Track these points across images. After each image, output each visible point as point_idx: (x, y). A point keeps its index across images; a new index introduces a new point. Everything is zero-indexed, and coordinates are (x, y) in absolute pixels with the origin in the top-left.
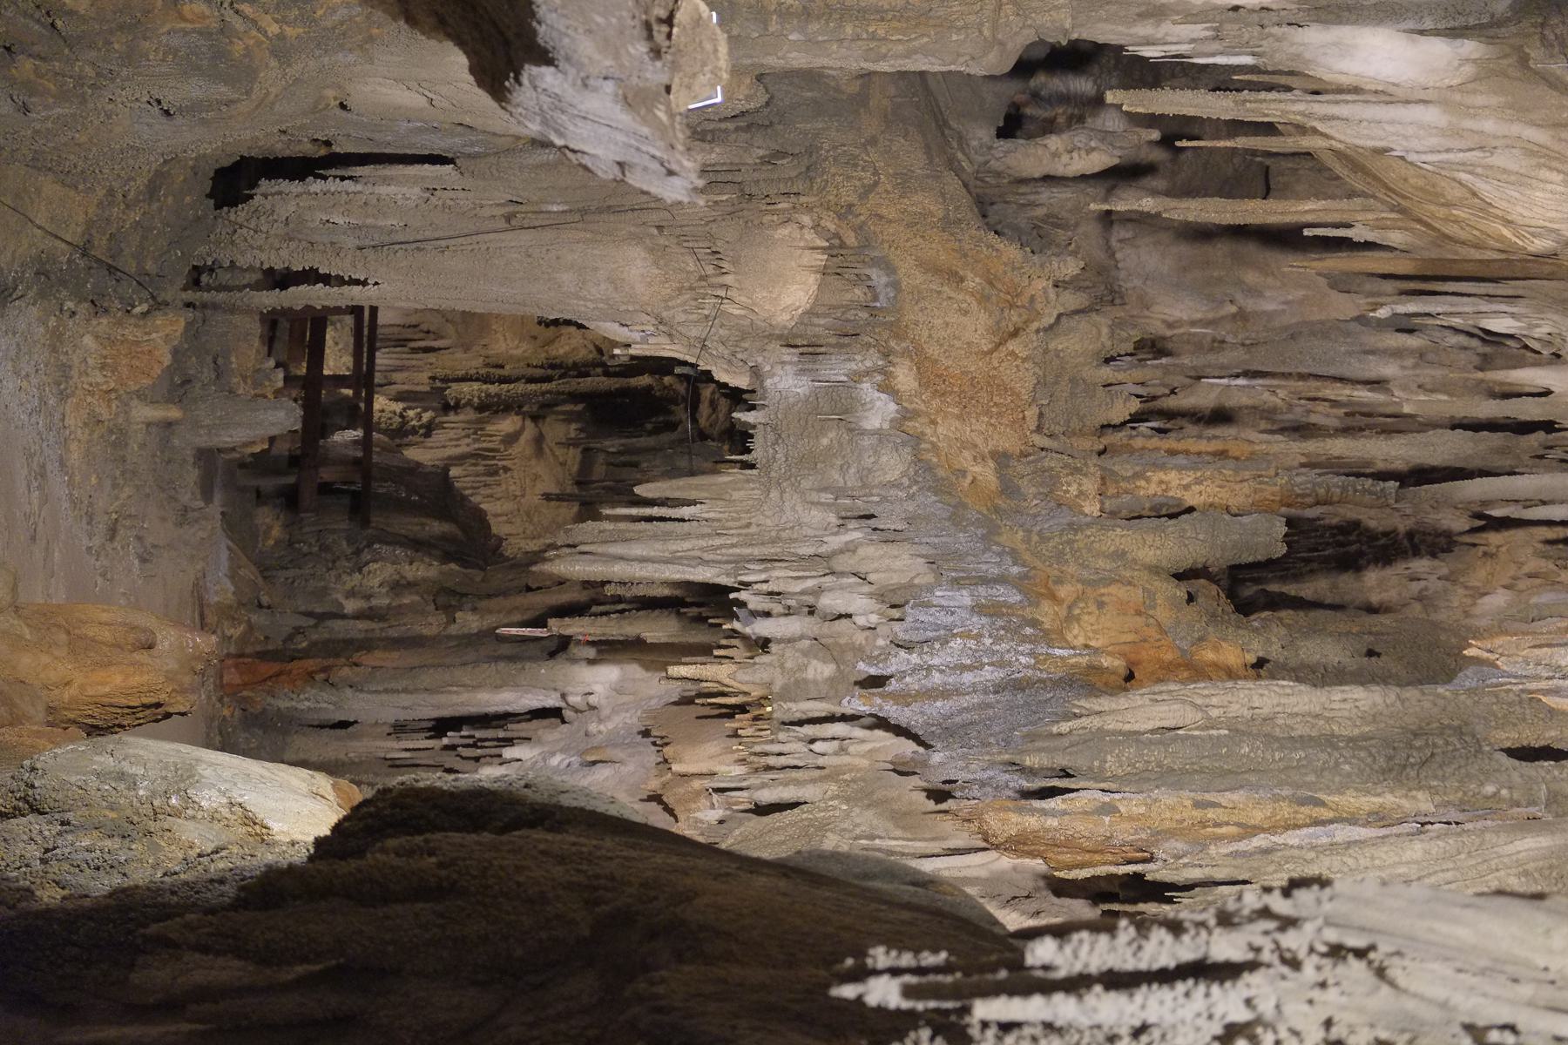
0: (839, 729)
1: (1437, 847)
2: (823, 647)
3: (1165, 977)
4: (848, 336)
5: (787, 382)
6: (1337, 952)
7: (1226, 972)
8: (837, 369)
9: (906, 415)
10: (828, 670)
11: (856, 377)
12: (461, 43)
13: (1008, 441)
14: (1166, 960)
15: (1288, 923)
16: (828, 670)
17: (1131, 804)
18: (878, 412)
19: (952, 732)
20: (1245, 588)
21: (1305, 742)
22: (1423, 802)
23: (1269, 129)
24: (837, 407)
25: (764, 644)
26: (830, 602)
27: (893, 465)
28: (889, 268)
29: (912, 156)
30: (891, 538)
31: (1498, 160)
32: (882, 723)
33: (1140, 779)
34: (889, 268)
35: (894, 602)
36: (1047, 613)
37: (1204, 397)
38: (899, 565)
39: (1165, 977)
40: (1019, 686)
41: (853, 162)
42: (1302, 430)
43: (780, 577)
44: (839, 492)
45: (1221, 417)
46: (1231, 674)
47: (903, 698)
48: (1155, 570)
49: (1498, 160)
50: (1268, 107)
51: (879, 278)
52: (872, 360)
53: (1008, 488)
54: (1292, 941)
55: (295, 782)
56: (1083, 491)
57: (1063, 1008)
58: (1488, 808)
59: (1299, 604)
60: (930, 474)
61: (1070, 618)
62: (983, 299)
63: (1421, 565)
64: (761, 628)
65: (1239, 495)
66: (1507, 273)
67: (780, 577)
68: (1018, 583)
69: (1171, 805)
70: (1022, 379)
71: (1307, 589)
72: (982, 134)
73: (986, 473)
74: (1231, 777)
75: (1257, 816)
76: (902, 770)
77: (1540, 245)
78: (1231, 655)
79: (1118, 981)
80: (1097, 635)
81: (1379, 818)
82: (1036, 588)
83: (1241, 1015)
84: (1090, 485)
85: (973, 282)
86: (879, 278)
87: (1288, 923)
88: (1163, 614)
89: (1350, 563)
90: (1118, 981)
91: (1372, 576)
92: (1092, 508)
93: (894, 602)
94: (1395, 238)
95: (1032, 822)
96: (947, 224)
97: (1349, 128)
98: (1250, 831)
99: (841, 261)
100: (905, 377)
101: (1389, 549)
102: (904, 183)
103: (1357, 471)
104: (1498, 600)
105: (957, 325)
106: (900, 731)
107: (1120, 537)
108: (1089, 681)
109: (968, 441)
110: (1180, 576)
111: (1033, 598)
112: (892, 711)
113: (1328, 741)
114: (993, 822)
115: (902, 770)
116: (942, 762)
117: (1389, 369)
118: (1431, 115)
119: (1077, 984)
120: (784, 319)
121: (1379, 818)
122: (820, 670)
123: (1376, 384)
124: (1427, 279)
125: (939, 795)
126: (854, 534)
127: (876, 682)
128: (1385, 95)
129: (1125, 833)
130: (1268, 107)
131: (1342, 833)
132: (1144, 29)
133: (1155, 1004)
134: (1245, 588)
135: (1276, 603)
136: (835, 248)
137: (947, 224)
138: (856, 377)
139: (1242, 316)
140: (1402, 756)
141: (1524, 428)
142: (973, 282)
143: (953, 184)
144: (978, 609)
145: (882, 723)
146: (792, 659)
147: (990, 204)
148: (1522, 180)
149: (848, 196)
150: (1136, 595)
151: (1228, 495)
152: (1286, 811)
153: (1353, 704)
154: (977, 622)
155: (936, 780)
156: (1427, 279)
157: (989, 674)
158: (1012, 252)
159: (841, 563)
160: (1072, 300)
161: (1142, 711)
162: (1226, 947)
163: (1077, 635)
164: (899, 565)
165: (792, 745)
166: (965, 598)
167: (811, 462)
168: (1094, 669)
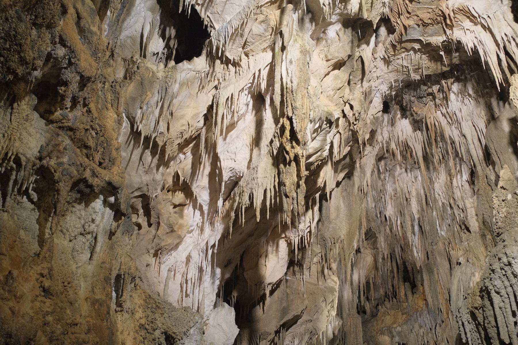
0: (437, 333)
1: (440, 268)
2: (427, 334)
3: (464, 329)
4: (391, 332)
5: (397, 339)
6: (459, 312)
7: (463, 323)
8: (395, 334)
9: (399, 325)
10: (430, 334)
11: (395, 331)
12: (211, 170)
13: (400, 313)
14: (463, 329)
15: (457, 316)
16: (430, 334)
17: (441, 301)
18: (399, 329)
19: (435, 320)
20: (414, 287)
21: (430, 282)
22: (435, 269)
23: (364, 286)
24: (399, 333)
25: (428, 342)
26: (422, 334)
27: (405, 327)
28: (383, 328)
29: (370, 325)
30: (413, 327)
31: (365, 264)
32: (435, 328)
33: (438, 300)
34: (383, 328)
35: (421, 327)
36: (420, 309)
37: (391, 288)
38: (416, 326)
39: (464, 329)
40: (429, 313)
41: (371, 332)
42: (394, 277)
43: (420, 340)
44: (409, 333)
45: (393, 286)
46: (424, 288)
47: (432, 326)
48: (413, 297)
49: (365, 264)
50: (361, 286)
51: (384, 329)
52: (393, 329)
53: (406, 313)
54: (458, 316)
55: (365, 57)
56: (405, 305)
57: (469, 339)
58: (435, 262)
59: (414, 279)
60: (406, 322)
61: (420, 306)
62: (385, 317)
63: (407, 264)
64: (426, 342)
65: (403, 287)
66: (376, 261)
67: (420, 340)
68: (417, 313)
69: (440, 297)
70: (393, 312)
71: (412, 278)
72: (366, 316)
73: (404, 316)
74: (436, 290)
75: (440, 287)
76: (441, 326)
77: (373, 258)
78: (421, 288)
79: (466, 334)
80: (421, 303)
81: (438, 274)
82: (417, 311)
83: (467, 322)
84: (404, 304)
85: (383, 318)
86: (384, 329)
87: (457, 316)
88: (418, 296)
89: (408, 271)
90: (466, 334)
91: (409, 269)
92: (407, 304)
93: (421, 327)
94: (373, 272)
95: (445, 312)
96: (377, 321)
97: (363, 281)
98: (442, 288)
99: (382, 333)
100: (395, 326)
101: (405, 267)
102: (373, 326)
103: (398, 272)
104: (410, 257)
105: (388, 320)
106: (436, 326)
107: (410, 301)
108: (427, 304)
109: (401, 318)
110: (413, 294)
111: (418, 311)
112: (434, 327)
113: (430, 279)
114: (445, 317)
115: (441, 326)
116: (439, 321)
117: (386, 269)
118: (361, 271)
119: (467, 338)
120: (390, 339)
121: (438, 274)
122: (430, 335)
123: (387, 270)
124: (376, 268)
125: (443, 322)
126: (413, 331)
127: (430, 329)
128: (359, 276)
129: (444, 302)
130: (361, 286)
131: (440, 278)
132: (355, 301)
133: (467, 330)
134: (414, 287)
135: (414, 281)
136: (381, 334)
137: (377, 321)
138: (395, 331)
139: (381, 284)
140: (430, 271)
141: (391, 256)
142: (383, 318)
143: (372, 320)
144: (420, 317)
145: (435, 328)
146: (429, 338)
147: (374, 315)
148: (367, 262)
149: (375, 332)
150: (416, 299)
151: (403, 290)
152: (439, 284)
153: (425, 277)
154: (422, 317)
155: (441, 322)
156: (376, 268)
157: (428, 316)
158: (379, 313)
159: (417, 332)
160: (384, 306)
161: (430, 300)
162: (460, 323)
163: (422, 306)
164: (416, 326)
165: (440, 338)
166: (419, 319)
167: (406, 336)
168: (425, 304)
